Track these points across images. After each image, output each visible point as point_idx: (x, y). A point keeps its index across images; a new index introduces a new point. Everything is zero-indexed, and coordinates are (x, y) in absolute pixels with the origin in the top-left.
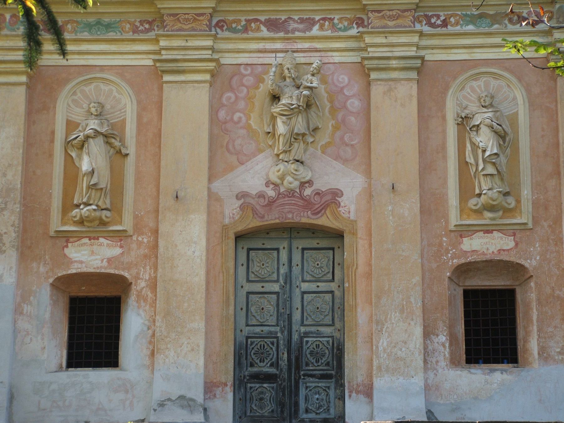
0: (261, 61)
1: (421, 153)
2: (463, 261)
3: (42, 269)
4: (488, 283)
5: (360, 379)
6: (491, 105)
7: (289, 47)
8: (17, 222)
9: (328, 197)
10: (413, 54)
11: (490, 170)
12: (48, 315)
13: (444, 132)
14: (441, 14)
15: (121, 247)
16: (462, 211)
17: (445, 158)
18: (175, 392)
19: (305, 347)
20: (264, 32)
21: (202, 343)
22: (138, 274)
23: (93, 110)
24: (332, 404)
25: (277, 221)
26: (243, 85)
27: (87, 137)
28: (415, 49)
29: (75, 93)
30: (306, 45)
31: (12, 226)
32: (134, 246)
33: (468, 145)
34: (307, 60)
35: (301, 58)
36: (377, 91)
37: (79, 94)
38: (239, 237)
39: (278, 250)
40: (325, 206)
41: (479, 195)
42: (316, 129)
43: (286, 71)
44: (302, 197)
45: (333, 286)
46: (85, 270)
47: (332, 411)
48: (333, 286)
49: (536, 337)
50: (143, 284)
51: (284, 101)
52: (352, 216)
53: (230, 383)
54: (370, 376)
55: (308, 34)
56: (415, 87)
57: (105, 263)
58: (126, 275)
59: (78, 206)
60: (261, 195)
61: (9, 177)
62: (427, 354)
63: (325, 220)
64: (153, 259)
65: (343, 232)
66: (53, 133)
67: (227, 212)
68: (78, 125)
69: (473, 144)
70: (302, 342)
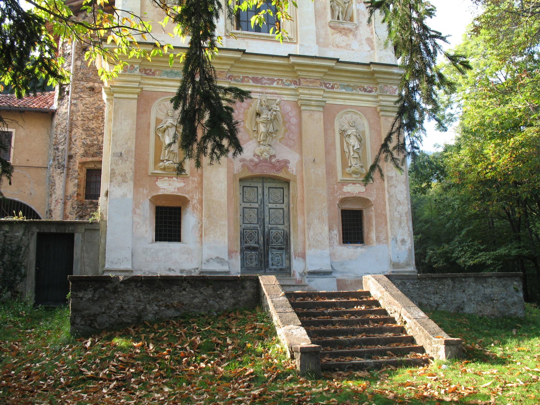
0: (272, 98)
1: (326, 145)
2: (344, 196)
3: (145, 192)
4: (348, 207)
5: (300, 250)
6: (354, 126)
7: (264, 91)
8: (133, 167)
9: (283, 164)
10: (137, 86)
11: (356, 155)
12: (148, 215)
13: (334, 137)
14: (241, 76)
15: (184, 182)
16: (343, 173)
17: (335, 148)
18: (214, 255)
19: (271, 235)
20: (251, 83)
21: (226, 231)
22: (193, 196)
23: (170, 114)
24: (284, 262)
25: (259, 174)
26: (242, 107)
27: (168, 127)
28: (138, 84)
29: (160, 105)
30: (272, 91)
31: (131, 169)
32: (190, 182)
33: (345, 144)
34: (274, 98)
35: (269, 97)
36: (305, 115)
37: (162, 106)
38: (241, 180)
39: (257, 187)
40: (281, 168)
41: (350, 167)
42: (277, 131)
43: (263, 102)
44: (271, 163)
45: (283, 206)
46: (166, 193)
47: (284, 265)
48: (283, 206)
49: (375, 232)
50: (195, 201)
51: (263, 116)
52: (294, 173)
53: (239, 251)
54: (304, 249)
55: (271, 86)
56: (322, 115)
57: (176, 190)
58: (187, 196)
59: (163, 161)
60: (251, 161)
61: (129, 144)
62: (330, 239)
63: (282, 175)
64: (200, 189)
65: (290, 181)
66: (149, 124)
67: (236, 168)
68: (161, 121)
69: (347, 143)
70: (269, 232)
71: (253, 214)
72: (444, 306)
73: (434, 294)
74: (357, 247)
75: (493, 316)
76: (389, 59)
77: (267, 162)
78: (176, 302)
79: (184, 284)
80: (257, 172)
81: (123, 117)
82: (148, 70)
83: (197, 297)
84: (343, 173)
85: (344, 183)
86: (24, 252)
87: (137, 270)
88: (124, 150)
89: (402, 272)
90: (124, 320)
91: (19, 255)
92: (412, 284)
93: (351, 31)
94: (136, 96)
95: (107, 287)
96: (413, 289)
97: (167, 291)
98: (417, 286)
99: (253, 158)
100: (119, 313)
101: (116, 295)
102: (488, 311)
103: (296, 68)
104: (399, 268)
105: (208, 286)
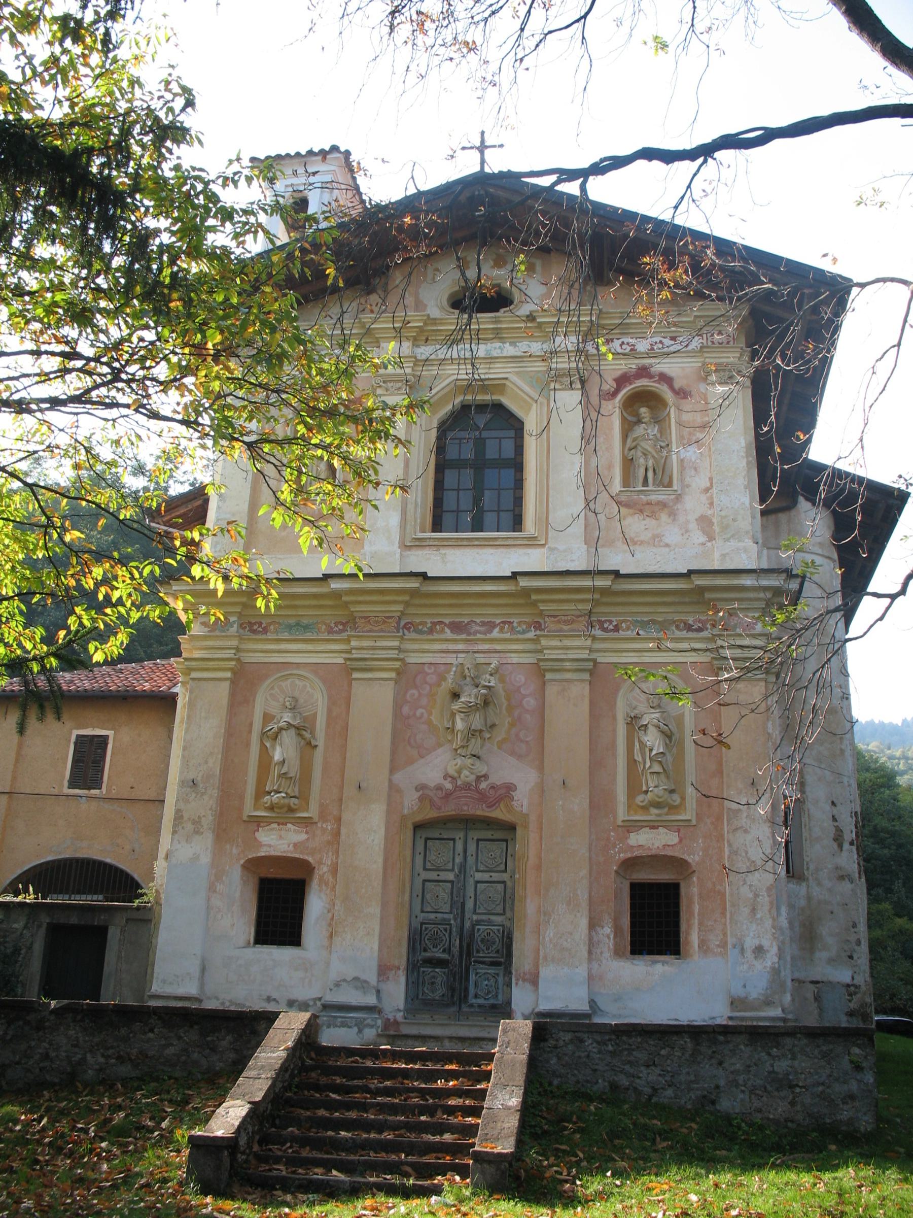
1: (592, 751)
2: (629, 855)
3: (235, 851)
7: (470, 648)
8: (214, 806)
9: (503, 791)
11: (657, 768)
12: (238, 895)
13: (614, 731)
15: (307, 833)
16: (629, 807)
17: (614, 756)
20: (448, 634)
22: (321, 859)
24: (500, 991)
25: (454, 813)
26: (426, 683)
29: (272, 688)
30: (486, 647)
31: (211, 809)
32: (318, 832)
35: (480, 658)
36: (551, 691)
39: (454, 840)
40: (499, 800)
41: (646, 792)
42: (493, 726)
44: (477, 790)
46: (273, 853)
47: (500, 997)
49: (696, 930)
50: (325, 869)
52: (525, 810)
54: (537, 966)
55: (489, 636)
56: (587, 687)
58: (310, 859)
59: (269, 793)
60: (439, 788)
62: (592, 945)
66: (251, 724)
68: (274, 717)
69: (640, 741)
70: (473, 930)
71: (444, 892)
72: (669, 1092)
73: (648, 1066)
74: (655, 962)
75: (792, 1121)
76: (744, 556)
77: (469, 789)
78: (135, 1051)
79: (152, 1021)
80: (449, 810)
81: (203, 714)
82: (255, 624)
83: (172, 1045)
84: (630, 806)
85: (631, 827)
86: (24, 958)
87: (209, 998)
88: (200, 774)
89: (752, 1019)
90: (48, 1077)
91: (16, 962)
92: (598, 1043)
93: (663, 505)
94: (228, 675)
95: (28, 1018)
96: (600, 1052)
97: (123, 1031)
98: (610, 1048)
99: (443, 781)
100: (41, 1065)
101: (41, 1033)
102: (779, 1108)
103: (534, 597)
104: (745, 1011)
105: (191, 1027)
